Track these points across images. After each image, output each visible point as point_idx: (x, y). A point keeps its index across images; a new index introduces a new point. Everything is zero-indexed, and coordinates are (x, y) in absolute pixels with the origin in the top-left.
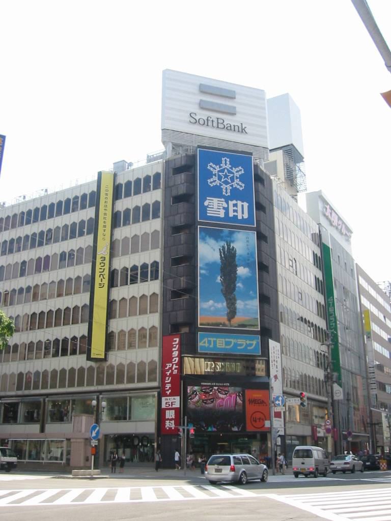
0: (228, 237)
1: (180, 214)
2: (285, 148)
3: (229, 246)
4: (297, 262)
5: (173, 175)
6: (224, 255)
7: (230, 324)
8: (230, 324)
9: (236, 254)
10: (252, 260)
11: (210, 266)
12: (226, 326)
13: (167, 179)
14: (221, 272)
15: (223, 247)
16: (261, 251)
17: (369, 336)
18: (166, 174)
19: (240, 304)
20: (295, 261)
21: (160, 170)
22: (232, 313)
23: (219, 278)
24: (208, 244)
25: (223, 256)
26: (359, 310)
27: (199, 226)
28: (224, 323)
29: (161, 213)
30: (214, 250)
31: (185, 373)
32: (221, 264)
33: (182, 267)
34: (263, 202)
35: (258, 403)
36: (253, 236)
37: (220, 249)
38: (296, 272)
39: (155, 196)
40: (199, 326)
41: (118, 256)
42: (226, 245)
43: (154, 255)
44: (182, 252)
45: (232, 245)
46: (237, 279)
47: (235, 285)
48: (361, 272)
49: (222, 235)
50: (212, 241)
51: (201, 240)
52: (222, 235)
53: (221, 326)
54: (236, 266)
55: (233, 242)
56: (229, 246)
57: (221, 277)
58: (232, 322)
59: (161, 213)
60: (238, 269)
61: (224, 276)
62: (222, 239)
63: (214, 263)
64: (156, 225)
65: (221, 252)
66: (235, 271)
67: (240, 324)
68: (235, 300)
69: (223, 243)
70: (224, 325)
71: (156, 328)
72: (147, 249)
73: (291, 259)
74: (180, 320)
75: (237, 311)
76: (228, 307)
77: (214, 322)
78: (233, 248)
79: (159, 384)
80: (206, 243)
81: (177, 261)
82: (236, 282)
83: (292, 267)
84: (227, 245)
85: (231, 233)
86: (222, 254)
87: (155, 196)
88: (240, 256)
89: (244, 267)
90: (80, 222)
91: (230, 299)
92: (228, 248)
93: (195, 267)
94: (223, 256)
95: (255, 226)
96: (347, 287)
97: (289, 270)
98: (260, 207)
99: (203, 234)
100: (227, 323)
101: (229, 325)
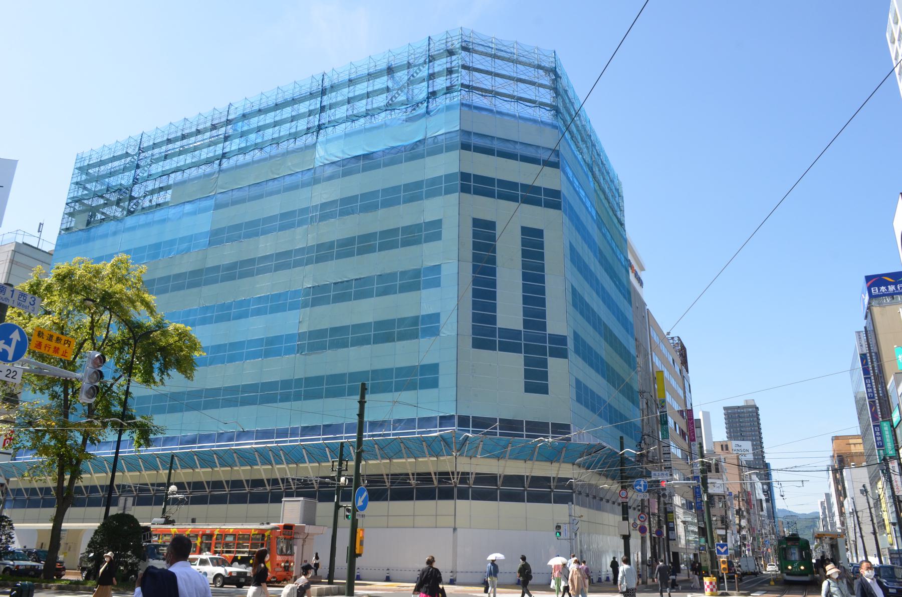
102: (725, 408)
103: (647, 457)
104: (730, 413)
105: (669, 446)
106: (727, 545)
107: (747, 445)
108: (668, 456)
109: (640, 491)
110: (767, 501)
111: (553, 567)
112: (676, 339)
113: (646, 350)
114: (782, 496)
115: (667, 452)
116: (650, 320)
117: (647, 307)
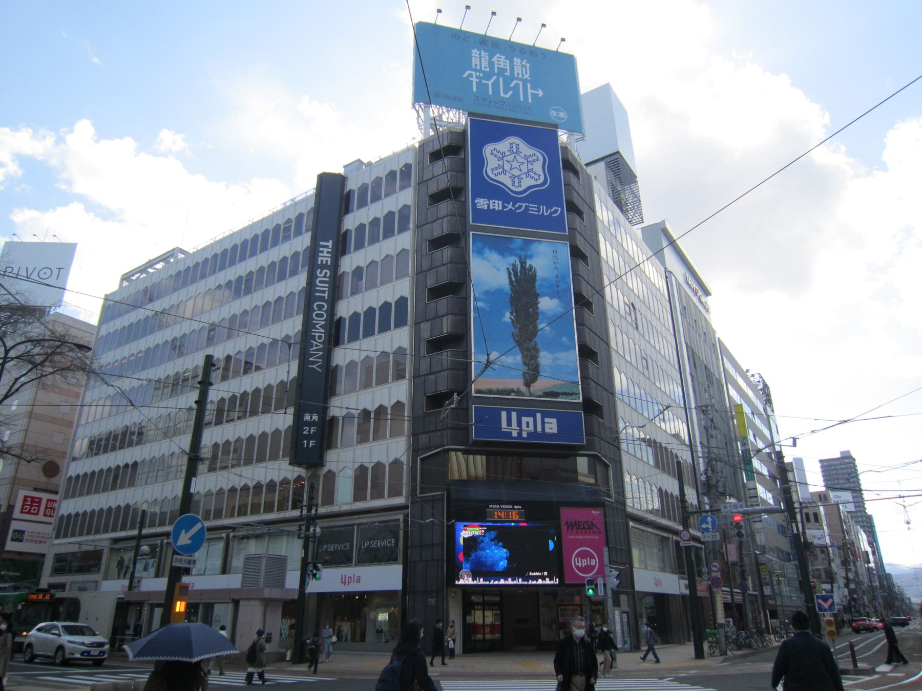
0: (522, 249)
1: (441, 218)
2: (609, 159)
3: (523, 263)
4: (637, 311)
5: (431, 162)
6: (515, 277)
7: (529, 391)
8: (529, 391)
9: (536, 276)
10: (563, 286)
11: (492, 295)
12: (523, 395)
13: (421, 170)
14: (512, 305)
15: (514, 266)
16: (583, 325)
17: (745, 441)
18: (420, 163)
19: (545, 359)
20: (634, 308)
21: (411, 160)
22: (532, 373)
23: (508, 315)
24: (489, 261)
25: (513, 279)
26: (728, 405)
27: (471, 233)
28: (518, 389)
29: (412, 225)
30: (498, 270)
31: (450, 478)
32: (510, 292)
33: (443, 304)
34: (587, 292)
35: (584, 528)
36: (564, 251)
37: (508, 269)
38: (636, 324)
39: (406, 197)
40: (474, 394)
41: (347, 298)
42: (518, 263)
43: (403, 288)
44: (444, 276)
45: (528, 263)
46: (540, 317)
47: (536, 327)
48: (725, 351)
49: (512, 246)
50: (494, 257)
51: (475, 254)
52: (512, 246)
53: (513, 394)
54: (537, 296)
55: (531, 257)
56: (523, 263)
57: (511, 314)
58: (532, 388)
59: (412, 225)
60: (540, 300)
61: (517, 312)
62: (511, 252)
63: (499, 292)
64: (405, 241)
65: (509, 274)
66: (536, 304)
67: (547, 391)
68: (537, 351)
69: (513, 259)
70: (518, 392)
71: (403, 405)
72: (390, 281)
73: (628, 303)
74: (443, 388)
75: (541, 369)
76: (525, 363)
77: (501, 387)
78: (531, 267)
79: (407, 498)
80: (484, 259)
81: (436, 292)
82: (538, 321)
83: (630, 314)
84: (521, 262)
85: (527, 243)
86: (512, 276)
87: (406, 197)
88: (544, 280)
89: (551, 298)
90: (274, 228)
91: (528, 350)
92: (523, 267)
93: (466, 299)
94: (513, 279)
95: (567, 234)
96: (710, 367)
97: (625, 318)
98: (582, 302)
99: (479, 245)
100: (523, 389)
101: (527, 393)
102: (821, 461)
103: (717, 487)
104: (826, 466)
105: (755, 489)
106: (832, 597)
107: (847, 496)
108: (755, 499)
109: (707, 530)
110: (874, 553)
111: (805, 612)
112: (757, 376)
113: (719, 381)
114: (908, 523)
115: (754, 495)
116: (722, 350)
117: (717, 336)
